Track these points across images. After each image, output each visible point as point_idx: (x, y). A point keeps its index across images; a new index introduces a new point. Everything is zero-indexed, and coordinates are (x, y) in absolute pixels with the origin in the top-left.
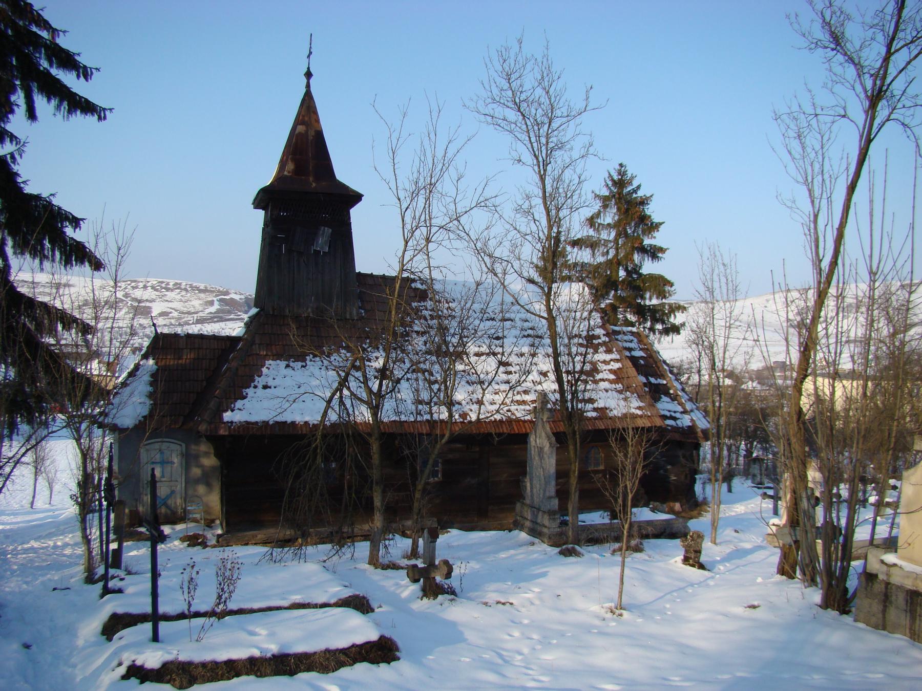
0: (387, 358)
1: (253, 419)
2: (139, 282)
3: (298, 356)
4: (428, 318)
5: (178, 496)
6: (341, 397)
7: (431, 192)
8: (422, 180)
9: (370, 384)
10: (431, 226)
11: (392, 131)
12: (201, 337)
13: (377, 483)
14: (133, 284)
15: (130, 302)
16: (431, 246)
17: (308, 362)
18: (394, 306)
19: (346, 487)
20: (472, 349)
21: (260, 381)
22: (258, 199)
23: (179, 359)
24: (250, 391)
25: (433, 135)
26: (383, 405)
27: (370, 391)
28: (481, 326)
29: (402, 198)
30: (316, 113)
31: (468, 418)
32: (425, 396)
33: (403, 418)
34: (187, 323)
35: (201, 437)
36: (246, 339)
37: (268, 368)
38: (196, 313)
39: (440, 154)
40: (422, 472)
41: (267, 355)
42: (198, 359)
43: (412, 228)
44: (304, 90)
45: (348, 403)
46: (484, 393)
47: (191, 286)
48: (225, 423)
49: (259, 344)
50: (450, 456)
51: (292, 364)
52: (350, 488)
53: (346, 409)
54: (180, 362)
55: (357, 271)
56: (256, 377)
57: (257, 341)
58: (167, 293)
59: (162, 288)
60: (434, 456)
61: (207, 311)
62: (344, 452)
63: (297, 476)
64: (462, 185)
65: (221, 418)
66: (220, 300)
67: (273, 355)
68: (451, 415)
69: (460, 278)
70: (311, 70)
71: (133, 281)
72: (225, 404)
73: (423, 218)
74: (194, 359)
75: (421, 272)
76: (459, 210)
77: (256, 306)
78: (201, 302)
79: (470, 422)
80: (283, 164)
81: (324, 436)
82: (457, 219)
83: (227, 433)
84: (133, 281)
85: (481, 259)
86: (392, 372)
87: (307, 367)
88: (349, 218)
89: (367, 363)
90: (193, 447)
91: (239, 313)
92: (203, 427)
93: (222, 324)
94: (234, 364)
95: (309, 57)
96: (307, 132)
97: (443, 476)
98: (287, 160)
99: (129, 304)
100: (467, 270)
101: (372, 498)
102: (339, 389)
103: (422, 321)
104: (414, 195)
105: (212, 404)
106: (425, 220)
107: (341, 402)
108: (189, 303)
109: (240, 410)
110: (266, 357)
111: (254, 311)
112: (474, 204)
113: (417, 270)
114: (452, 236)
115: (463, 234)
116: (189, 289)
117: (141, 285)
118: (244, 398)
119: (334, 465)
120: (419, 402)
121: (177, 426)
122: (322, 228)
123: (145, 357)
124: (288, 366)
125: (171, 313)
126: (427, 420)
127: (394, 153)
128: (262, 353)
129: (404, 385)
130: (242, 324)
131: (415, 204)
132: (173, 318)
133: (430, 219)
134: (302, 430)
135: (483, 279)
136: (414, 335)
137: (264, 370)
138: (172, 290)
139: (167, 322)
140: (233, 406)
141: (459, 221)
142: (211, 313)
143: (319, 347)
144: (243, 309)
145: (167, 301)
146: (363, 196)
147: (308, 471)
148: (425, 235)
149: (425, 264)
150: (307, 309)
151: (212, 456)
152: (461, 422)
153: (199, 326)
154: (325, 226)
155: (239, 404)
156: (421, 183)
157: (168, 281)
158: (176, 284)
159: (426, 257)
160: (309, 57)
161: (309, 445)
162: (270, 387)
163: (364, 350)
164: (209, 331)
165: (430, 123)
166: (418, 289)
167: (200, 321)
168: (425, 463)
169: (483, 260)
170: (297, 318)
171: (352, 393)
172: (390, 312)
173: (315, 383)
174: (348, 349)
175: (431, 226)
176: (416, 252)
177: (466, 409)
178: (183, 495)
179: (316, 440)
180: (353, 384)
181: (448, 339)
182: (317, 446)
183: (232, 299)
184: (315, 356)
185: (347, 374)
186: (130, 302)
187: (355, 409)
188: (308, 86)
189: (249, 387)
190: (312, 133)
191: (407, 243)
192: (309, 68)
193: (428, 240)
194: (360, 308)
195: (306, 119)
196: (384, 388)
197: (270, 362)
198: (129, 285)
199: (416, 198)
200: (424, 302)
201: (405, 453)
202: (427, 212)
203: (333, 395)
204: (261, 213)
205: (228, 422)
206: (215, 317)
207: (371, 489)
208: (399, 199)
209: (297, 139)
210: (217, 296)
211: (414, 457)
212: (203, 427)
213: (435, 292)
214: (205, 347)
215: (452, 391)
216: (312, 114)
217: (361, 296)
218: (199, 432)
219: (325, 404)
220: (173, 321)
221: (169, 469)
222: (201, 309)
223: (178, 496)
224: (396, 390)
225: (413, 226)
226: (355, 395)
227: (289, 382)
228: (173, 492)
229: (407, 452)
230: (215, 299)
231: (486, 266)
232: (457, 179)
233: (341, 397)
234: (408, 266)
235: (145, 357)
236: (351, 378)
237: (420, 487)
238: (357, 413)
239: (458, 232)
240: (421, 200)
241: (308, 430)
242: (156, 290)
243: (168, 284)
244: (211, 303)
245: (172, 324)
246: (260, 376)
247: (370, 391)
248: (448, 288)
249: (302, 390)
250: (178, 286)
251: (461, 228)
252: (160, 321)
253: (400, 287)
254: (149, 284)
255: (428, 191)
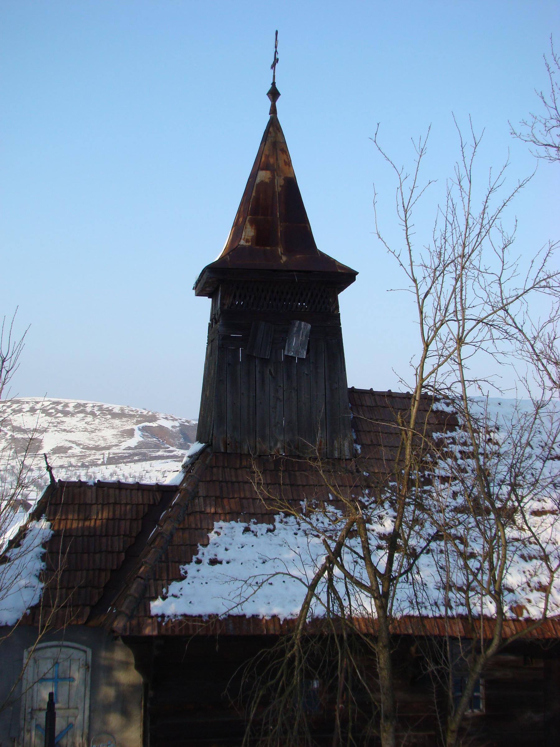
0: (399, 519)
1: (195, 610)
2: (23, 403)
3: (263, 515)
4: (459, 455)
5: (78, 733)
6: (330, 580)
7: (463, 268)
8: (449, 250)
9: (374, 559)
10: (464, 319)
11: (403, 177)
12: (119, 486)
13: (386, 717)
14: (15, 406)
15: (10, 433)
16: (466, 350)
17: (277, 524)
18: (409, 442)
19: (338, 722)
20: (531, 505)
21: (205, 553)
22: (202, 282)
23: (86, 519)
24: (191, 569)
25: (465, 183)
26: (394, 594)
27: (374, 571)
28: (546, 472)
29: (419, 279)
30: (285, 151)
31: (525, 614)
32: (459, 578)
33: (428, 612)
34: (94, 464)
35: (116, 638)
36: (185, 489)
37: (218, 533)
38: (108, 448)
39: (476, 212)
40: (457, 700)
41: (216, 513)
42: (113, 519)
43: (435, 324)
44: (268, 118)
45: (340, 588)
46: (552, 577)
47: (101, 408)
48: (152, 617)
49: (205, 497)
50: (498, 674)
51: (253, 527)
52: (344, 723)
53: (339, 598)
54: (87, 523)
55: (349, 386)
56: (200, 547)
57: (202, 492)
58: (64, 419)
59: (58, 411)
60: (475, 676)
61: (124, 445)
62: (336, 667)
63: (264, 703)
64: (510, 255)
65: (147, 609)
66: (144, 429)
67: (225, 514)
68: (500, 610)
69: (509, 396)
70: (277, 86)
71: (14, 402)
72: (153, 589)
73: (451, 309)
74: (108, 519)
75: (449, 389)
76: (506, 294)
77: (200, 439)
78: (115, 432)
79: (529, 620)
80: (238, 228)
81: (305, 640)
82: (504, 308)
83: (155, 633)
84: (14, 402)
85: (542, 368)
86: (406, 541)
87: (276, 532)
88: (337, 307)
89: (368, 525)
90: (104, 654)
91: (171, 448)
92: (119, 624)
93: (146, 465)
94: (167, 527)
95: (273, 66)
96: (273, 179)
97: (487, 706)
98: (244, 222)
99: (8, 436)
100: (520, 385)
101: (378, 739)
102: (328, 567)
103: (449, 460)
104: (438, 273)
105: (134, 589)
106: (456, 312)
107: (331, 587)
108: (97, 433)
109: (175, 596)
110: (215, 517)
111: (196, 447)
112: (530, 284)
113: (443, 386)
114: (496, 333)
115: (513, 331)
116: (98, 413)
117: (26, 407)
118: (182, 578)
119: (316, 684)
120: (448, 586)
121: (80, 623)
122: (297, 323)
123: (36, 516)
124: (247, 530)
125: (70, 448)
126: (460, 616)
127: (406, 211)
128: (208, 510)
129: (424, 560)
130: (179, 466)
131: (439, 287)
132: (73, 456)
133: (463, 309)
134: (268, 630)
135: (547, 398)
136: (437, 482)
137: (212, 536)
138: (73, 415)
139: (64, 462)
140: (164, 590)
141: (506, 311)
142: (129, 448)
143: (294, 502)
144: (177, 442)
145: (65, 430)
146: (357, 273)
147: (280, 696)
148: (456, 333)
149: (455, 377)
150: (276, 444)
151: (133, 667)
152: (514, 620)
153: (112, 468)
154: (301, 320)
155: (174, 587)
156: (448, 255)
157: (66, 401)
158: (78, 406)
159: (457, 367)
160: (273, 66)
161: (282, 653)
162: (221, 563)
163: (364, 507)
164: (127, 474)
165: (461, 164)
166: (443, 412)
167: (113, 460)
168: (460, 686)
169: (546, 370)
170: (261, 458)
171: (347, 575)
172: (403, 449)
173: (289, 555)
174: (336, 503)
175: (464, 319)
176: (442, 359)
177: (521, 597)
178: (86, 730)
179: (292, 646)
180: (347, 558)
181: (495, 490)
182: (293, 657)
183: (161, 427)
184: (287, 515)
185: (340, 545)
186: (10, 433)
187: (352, 598)
188: (273, 111)
189: (189, 562)
190: (280, 181)
191: (427, 345)
192: (274, 84)
193: (460, 341)
194: (356, 442)
195: (272, 161)
196: (395, 566)
197: (221, 523)
198: (9, 407)
199: (440, 279)
200: (451, 431)
201: (430, 669)
202: (458, 300)
203: (318, 576)
204: (206, 303)
205: (157, 616)
206: (136, 454)
207: (377, 725)
208: (415, 281)
209: (258, 192)
210: (138, 422)
211: (443, 675)
212: (119, 624)
213: (468, 416)
214: (124, 501)
215: (501, 572)
216: (279, 152)
217: (355, 425)
218: (113, 631)
219: (306, 590)
220: (73, 461)
221: (66, 688)
222: (115, 442)
223: (78, 733)
224: (415, 570)
225: (437, 320)
226: (351, 577)
227: (249, 554)
228: (70, 726)
229: (432, 667)
230: (136, 427)
231: (550, 378)
232: (502, 246)
233: (330, 580)
234: (430, 381)
235: (36, 516)
236: (344, 550)
237: (453, 726)
238: (354, 604)
239: (506, 327)
240: (449, 280)
241: (277, 627)
242: (50, 415)
243: (66, 405)
244: (130, 433)
245: (71, 465)
246: (205, 545)
247: (374, 571)
248: (492, 409)
249: (269, 569)
250: (81, 408)
251: (510, 322)
252: (55, 461)
253: (418, 410)
254: (38, 406)
255: (459, 267)
